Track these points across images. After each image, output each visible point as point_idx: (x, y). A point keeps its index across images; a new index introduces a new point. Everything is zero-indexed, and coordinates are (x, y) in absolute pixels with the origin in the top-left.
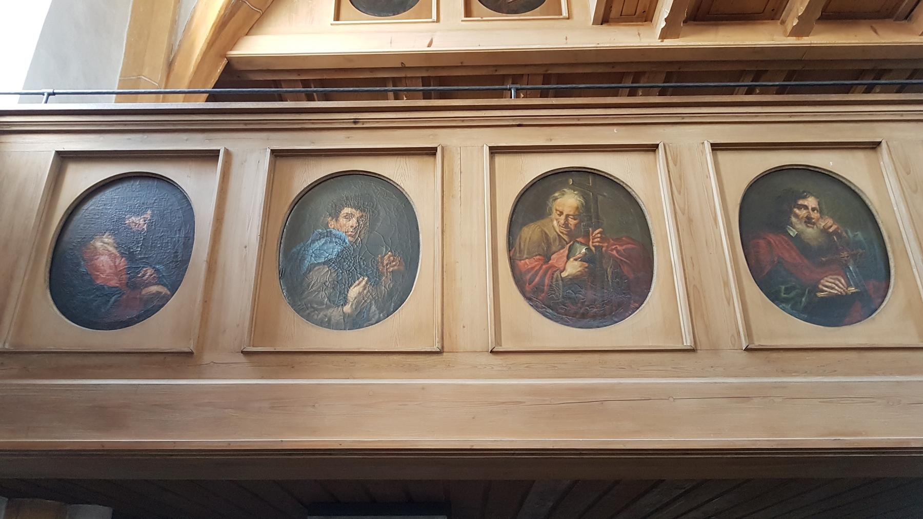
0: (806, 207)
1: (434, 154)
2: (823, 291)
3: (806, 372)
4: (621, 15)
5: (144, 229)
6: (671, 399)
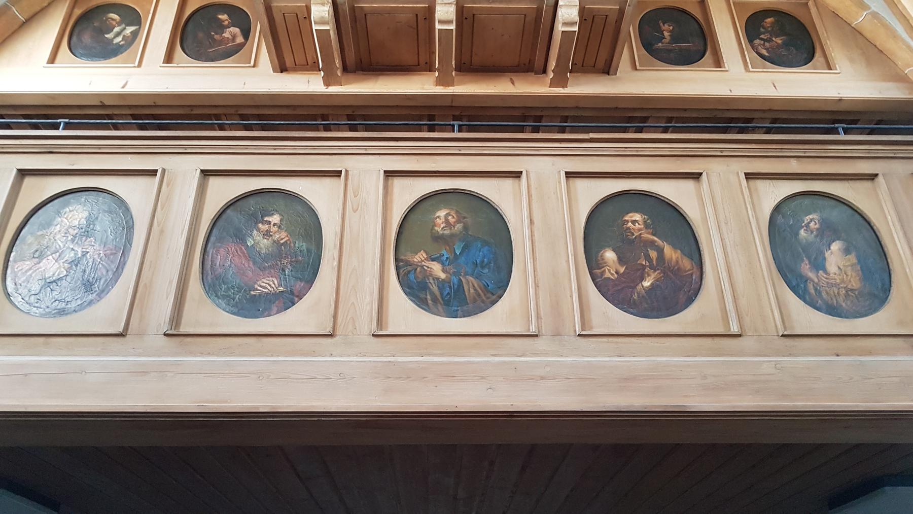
0: (269, 223)
1: (340, 176)
2: (257, 290)
3: (209, 353)
4: (582, 66)
5: (633, 235)
6: (84, 373)
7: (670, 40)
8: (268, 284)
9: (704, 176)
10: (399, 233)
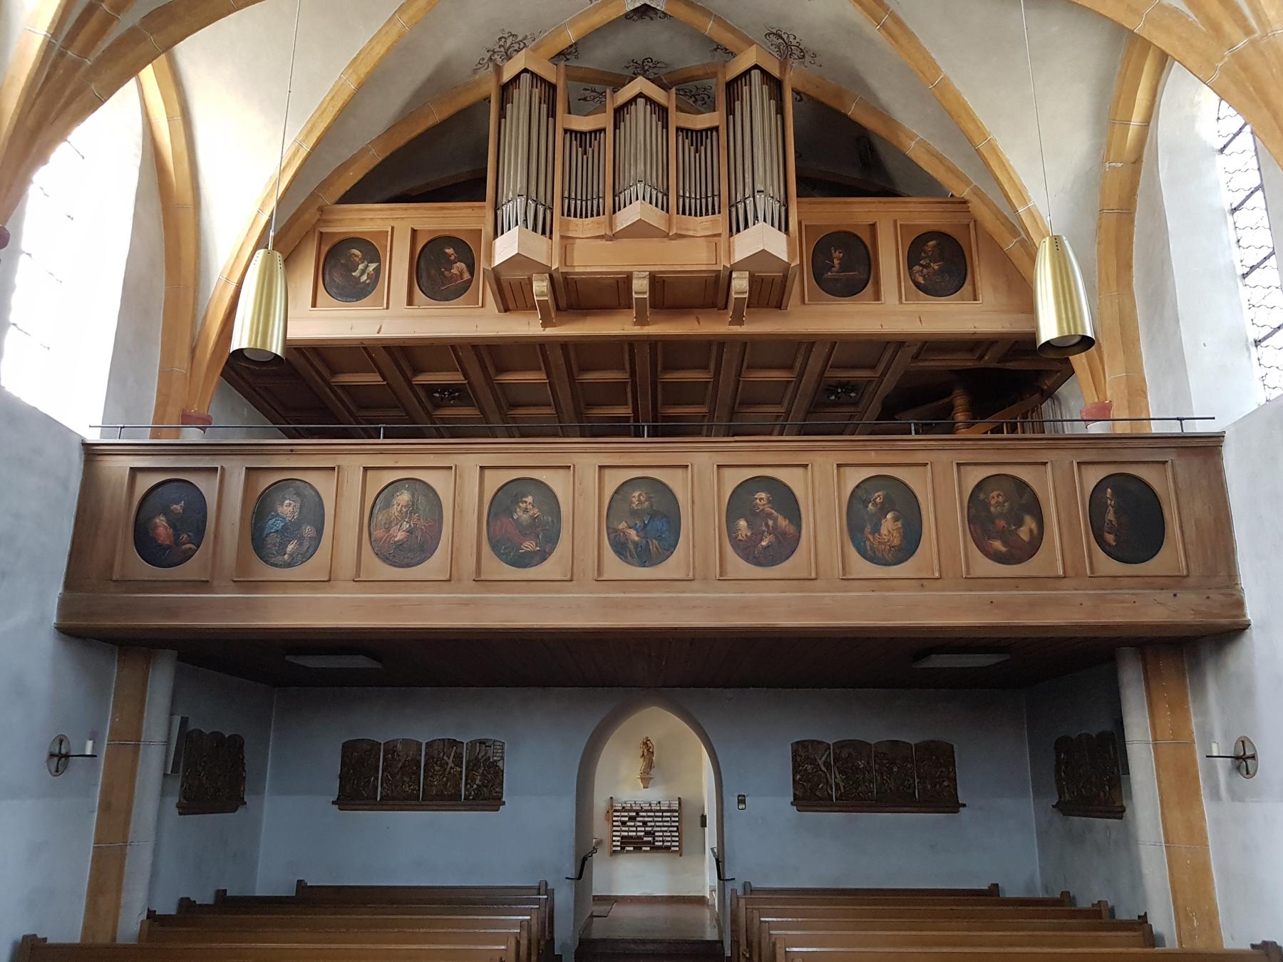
0: (526, 502)
7: (840, 268)
8: (529, 545)
9: (810, 466)
10: (608, 509)
